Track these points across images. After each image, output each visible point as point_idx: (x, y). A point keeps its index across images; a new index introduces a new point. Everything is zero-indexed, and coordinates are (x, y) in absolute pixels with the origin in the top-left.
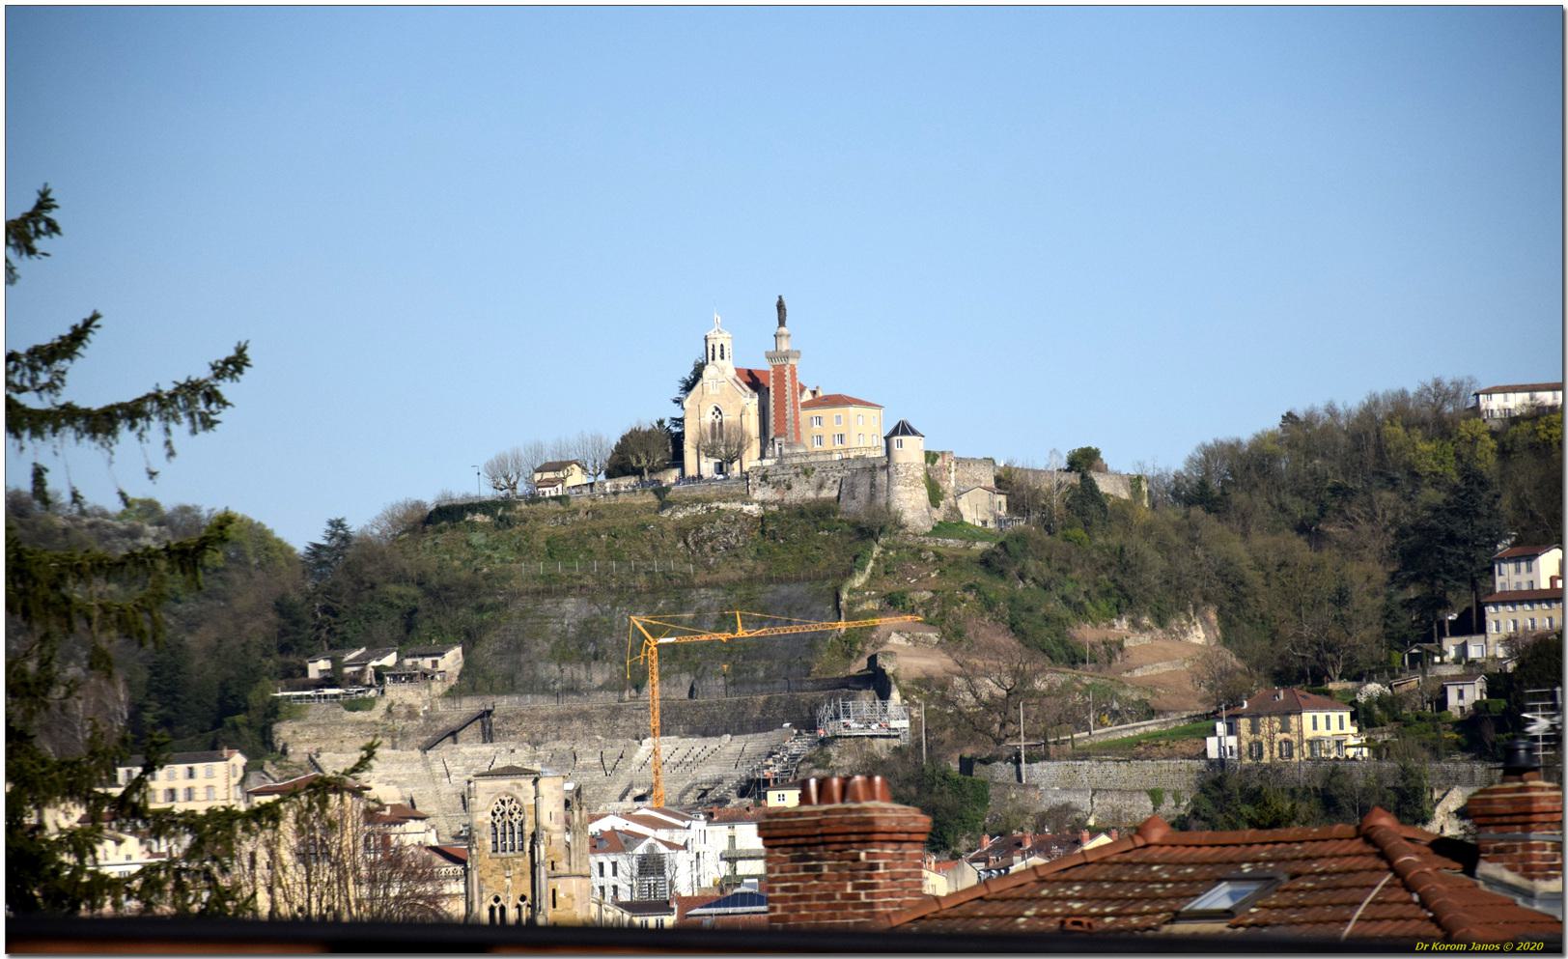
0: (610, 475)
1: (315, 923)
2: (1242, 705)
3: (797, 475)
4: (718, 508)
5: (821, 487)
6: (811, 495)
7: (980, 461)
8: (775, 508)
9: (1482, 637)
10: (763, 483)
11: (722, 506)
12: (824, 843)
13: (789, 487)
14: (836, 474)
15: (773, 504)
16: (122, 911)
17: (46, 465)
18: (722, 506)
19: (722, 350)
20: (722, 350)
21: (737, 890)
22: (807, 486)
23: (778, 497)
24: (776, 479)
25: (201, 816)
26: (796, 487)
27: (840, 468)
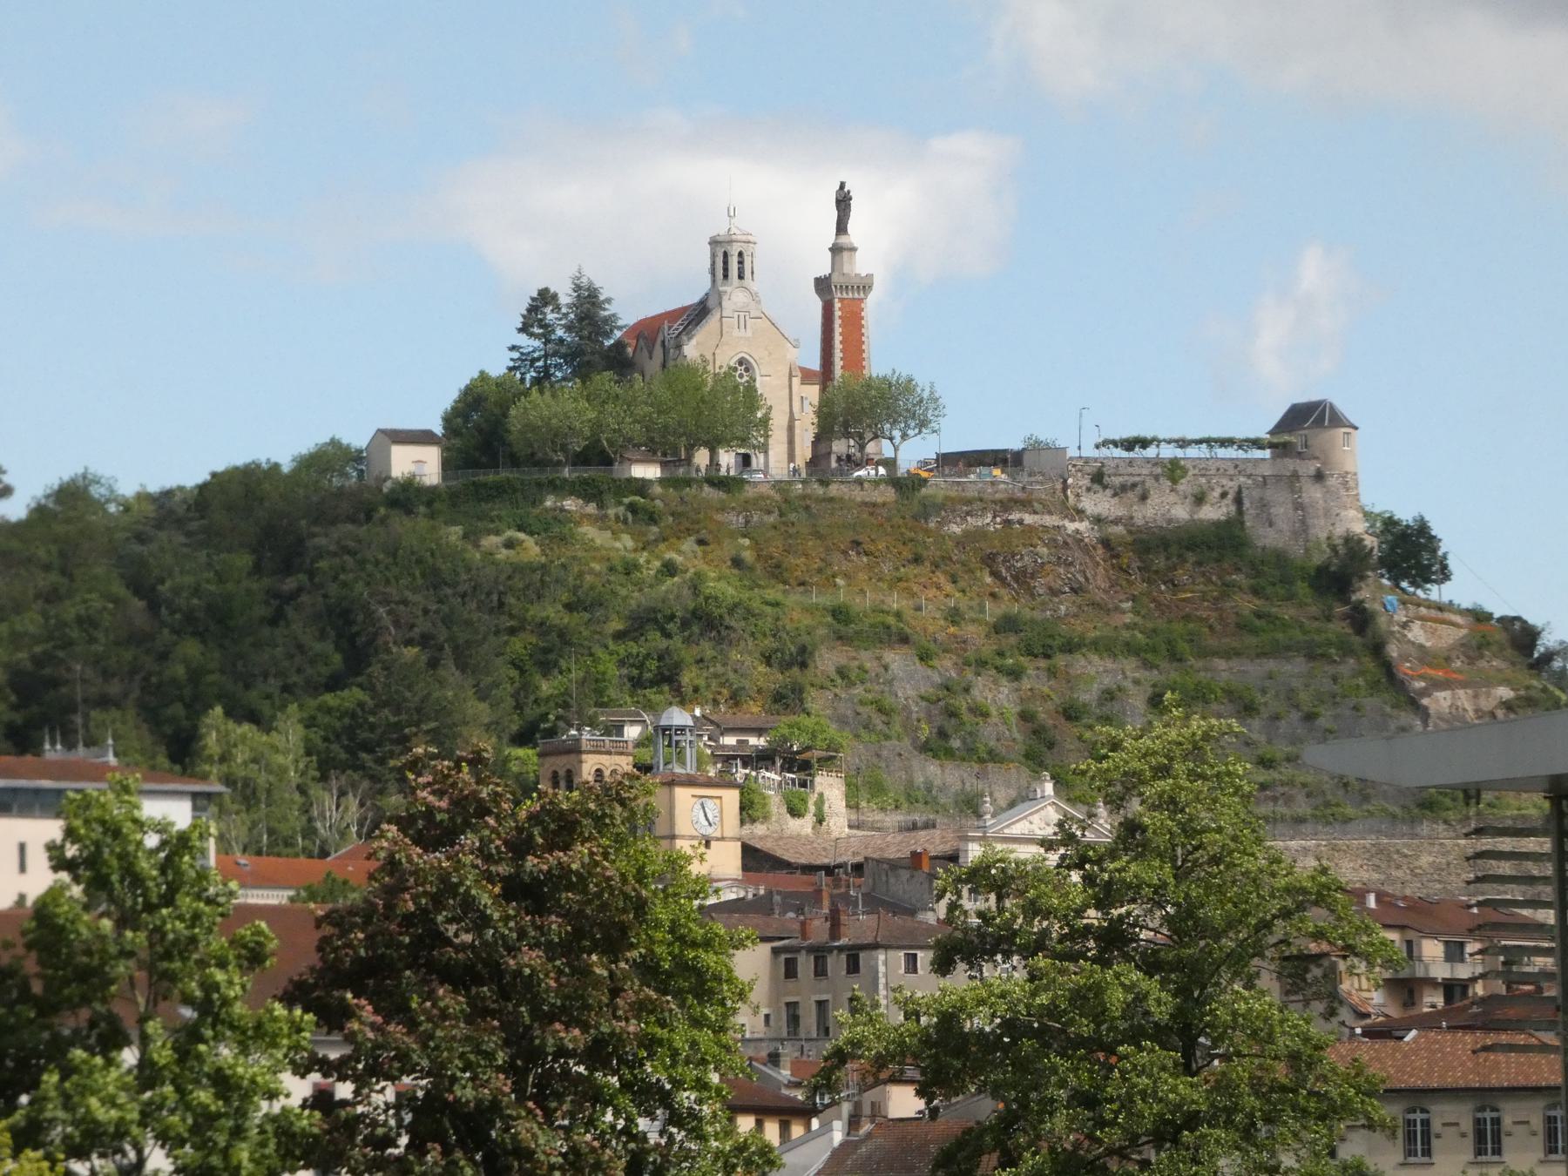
0: (289, 1000)
1: (301, 1003)
2: (318, 998)
3: (1157, 478)
4: (1021, 522)
5: (1199, 499)
6: (1181, 512)
10: (1096, 487)
11: (1029, 519)
13: (1144, 498)
14: (1224, 481)
15: (1117, 521)
16: (953, 790)
18: (1029, 519)
19: (741, 262)
20: (741, 262)
22: (1172, 498)
24: (1117, 481)
26: (1154, 500)
27: (1231, 471)
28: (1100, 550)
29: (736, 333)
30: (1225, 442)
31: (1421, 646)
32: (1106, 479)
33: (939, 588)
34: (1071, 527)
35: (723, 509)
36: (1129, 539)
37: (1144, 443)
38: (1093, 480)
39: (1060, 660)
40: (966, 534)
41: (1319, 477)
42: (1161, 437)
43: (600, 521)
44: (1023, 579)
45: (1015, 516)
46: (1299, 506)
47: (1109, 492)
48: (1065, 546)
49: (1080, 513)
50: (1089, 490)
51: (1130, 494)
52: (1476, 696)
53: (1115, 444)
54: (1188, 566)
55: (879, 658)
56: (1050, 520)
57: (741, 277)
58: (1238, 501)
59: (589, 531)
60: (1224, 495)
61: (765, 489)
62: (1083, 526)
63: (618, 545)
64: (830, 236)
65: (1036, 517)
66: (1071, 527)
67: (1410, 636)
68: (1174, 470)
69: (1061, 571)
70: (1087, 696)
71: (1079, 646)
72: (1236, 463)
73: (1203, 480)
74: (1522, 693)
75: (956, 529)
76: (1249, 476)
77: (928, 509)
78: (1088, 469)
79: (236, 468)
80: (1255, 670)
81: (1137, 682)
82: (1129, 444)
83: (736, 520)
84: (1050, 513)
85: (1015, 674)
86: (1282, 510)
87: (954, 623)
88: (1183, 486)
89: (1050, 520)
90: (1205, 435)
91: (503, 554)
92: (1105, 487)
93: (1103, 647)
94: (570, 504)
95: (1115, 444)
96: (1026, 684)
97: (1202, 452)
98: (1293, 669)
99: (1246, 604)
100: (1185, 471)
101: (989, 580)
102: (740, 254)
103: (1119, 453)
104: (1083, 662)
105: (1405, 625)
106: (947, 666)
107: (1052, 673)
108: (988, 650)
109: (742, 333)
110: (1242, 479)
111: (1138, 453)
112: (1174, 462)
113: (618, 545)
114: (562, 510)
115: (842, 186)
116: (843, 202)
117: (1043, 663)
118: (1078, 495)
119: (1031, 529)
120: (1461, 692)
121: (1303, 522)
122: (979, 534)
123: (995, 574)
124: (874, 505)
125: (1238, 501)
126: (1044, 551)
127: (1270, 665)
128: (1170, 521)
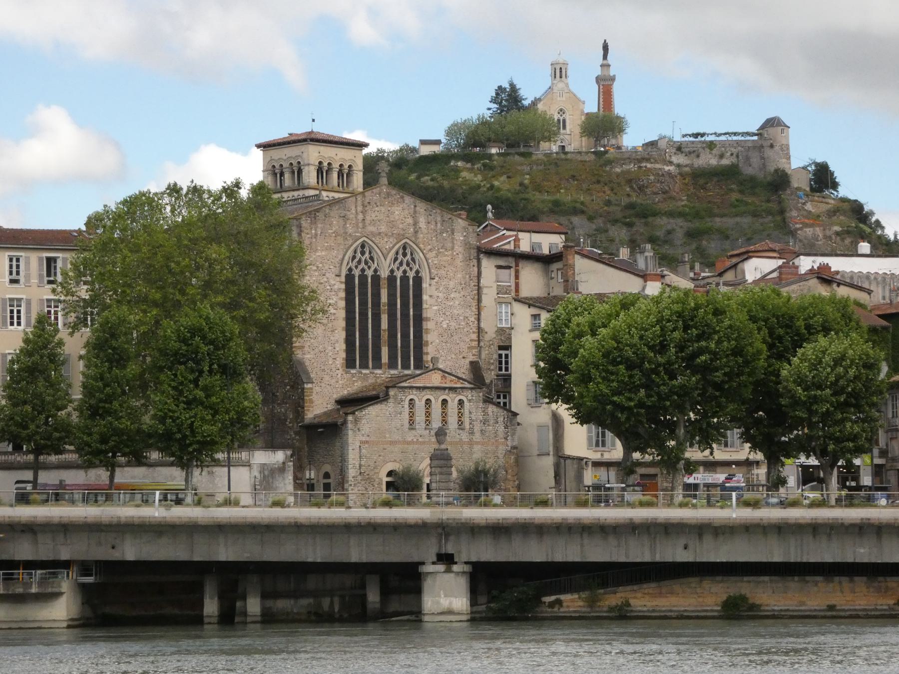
3: (704, 148)
4: (646, 167)
5: (722, 156)
6: (714, 162)
7: (711, 134)
8: (687, 169)
9: (533, 241)
10: (678, 152)
11: (649, 166)
12: (744, 654)
13: (698, 156)
15: (686, 166)
17: (418, 141)
18: (649, 166)
20: (561, 72)
21: (44, 571)
22: (710, 156)
23: (688, 162)
24: (687, 150)
25: (471, 568)
26: (702, 156)
28: (679, 177)
29: (559, 99)
30: (735, 134)
31: (810, 211)
32: (683, 150)
33: (604, 192)
34: (667, 168)
35: (522, 164)
36: (691, 172)
37: (703, 135)
38: (677, 150)
39: (650, 219)
40: (622, 172)
41: (772, 146)
42: (707, 132)
43: (471, 170)
44: (641, 188)
45: (643, 164)
46: (762, 158)
47: (684, 154)
48: (661, 176)
49: (671, 163)
50: (675, 153)
51: (692, 155)
52: (824, 230)
53: (690, 136)
54: (713, 183)
55: (569, 220)
56: (658, 166)
57: (561, 77)
58: (737, 156)
59: (464, 174)
60: (732, 154)
61: (540, 157)
62: (672, 168)
63: (476, 179)
64: (600, 61)
65: (652, 165)
66: (667, 168)
67: (806, 208)
68: (711, 145)
69: (658, 185)
70: (660, 233)
71: (657, 214)
72: (737, 142)
73: (723, 149)
74: (846, 229)
75: (618, 170)
76: (742, 147)
77: (609, 162)
78: (675, 146)
79: (229, 150)
80: (730, 222)
81: (681, 227)
82: (696, 135)
83: (527, 169)
84: (658, 163)
85: (630, 225)
86: (755, 160)
87: (606, 205)
88: (715, 151)
89: (658, 166)
90: (735, 131)
91: (431, 183)
92: (682, 152)
93: (671, 214)
94: (459, 164)
95: (690, 136)
96: (635, 229)
97: (723, 138)
98: (746, 221)
99: (735, 196)
100: (715, 146)
101: (628, 189)
102: (561, 68)
103: (692, 139)
104: (659, 220)
105: (804, 204)
106: (600, 222)
107: (646, 224)
108: (619, 215)
109: (561, 98)
110: (740, 148)
111: (699, 139)
112: (711, 142)
113: (476, 179)
114: (457, 166)
115: (605, 41)
116: (606, 48)
117: (643, 220)
118: (670, 156)
119: (650, 170)
120: (817, 229)
121: (764, 164)
122: (628, 172)
123: (631, 187)
124: (585, 161)
125: (737, 156)
126: (652, 178)
127: (738, 219)
128: (709, 165)
